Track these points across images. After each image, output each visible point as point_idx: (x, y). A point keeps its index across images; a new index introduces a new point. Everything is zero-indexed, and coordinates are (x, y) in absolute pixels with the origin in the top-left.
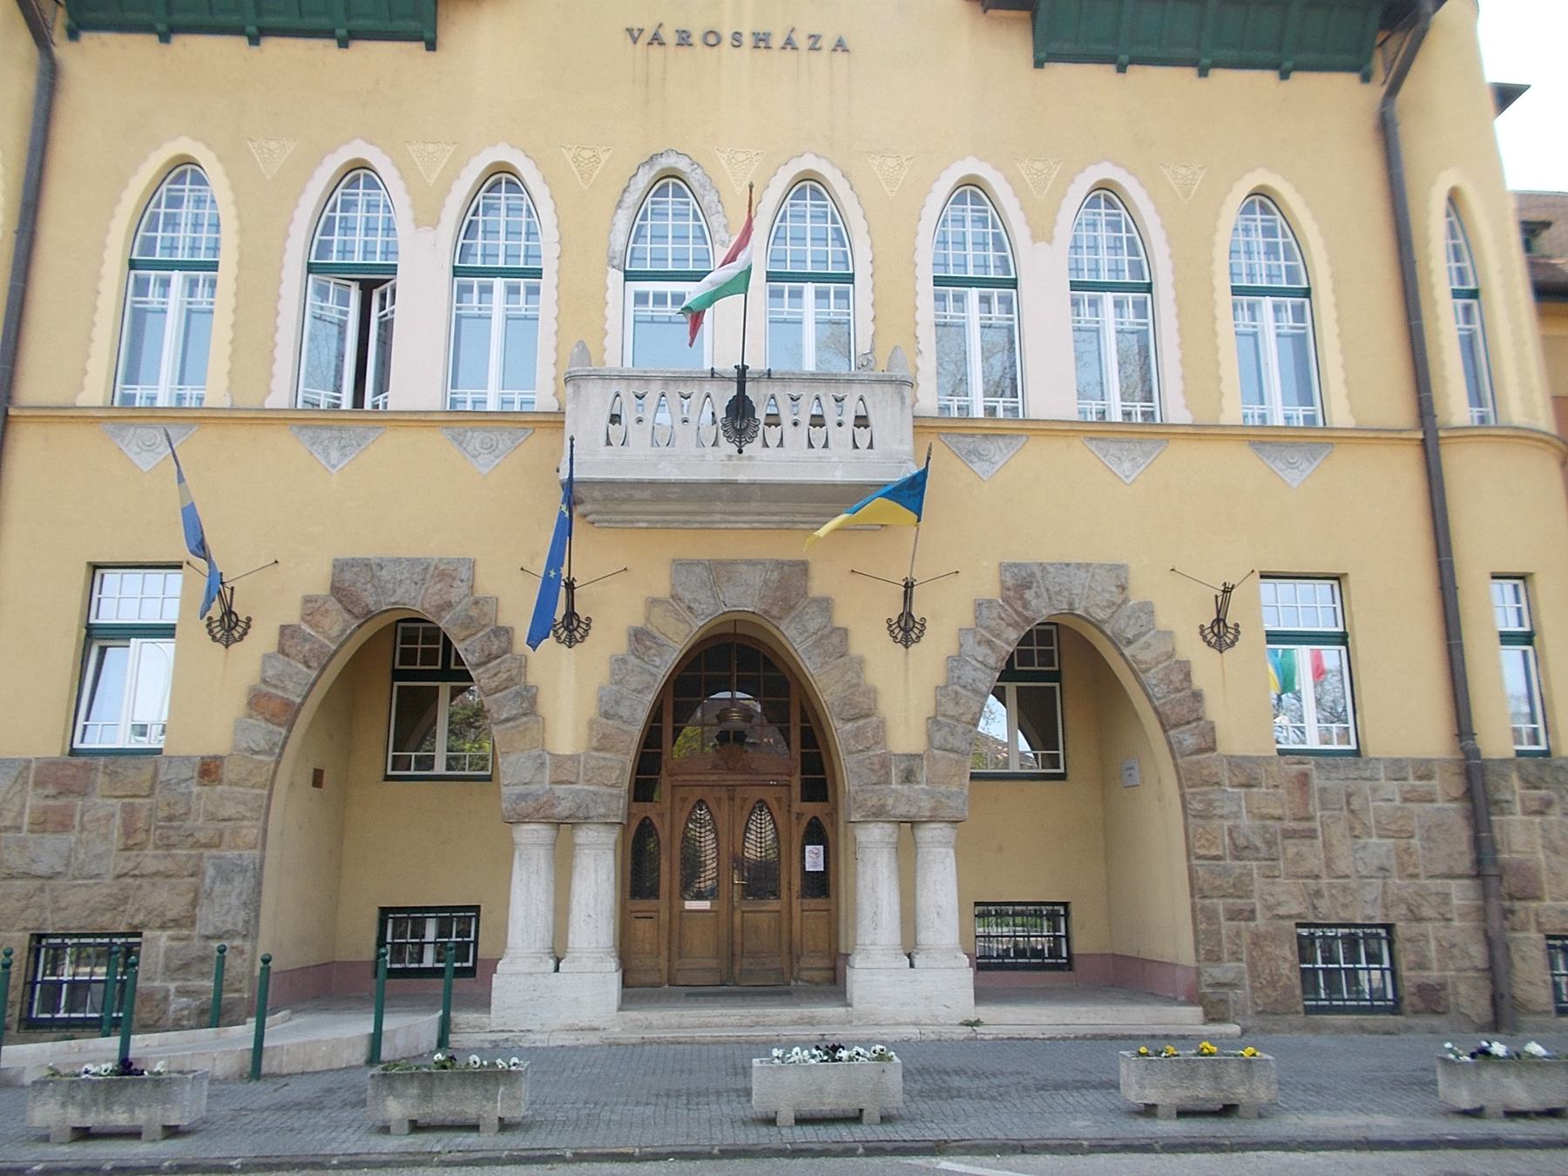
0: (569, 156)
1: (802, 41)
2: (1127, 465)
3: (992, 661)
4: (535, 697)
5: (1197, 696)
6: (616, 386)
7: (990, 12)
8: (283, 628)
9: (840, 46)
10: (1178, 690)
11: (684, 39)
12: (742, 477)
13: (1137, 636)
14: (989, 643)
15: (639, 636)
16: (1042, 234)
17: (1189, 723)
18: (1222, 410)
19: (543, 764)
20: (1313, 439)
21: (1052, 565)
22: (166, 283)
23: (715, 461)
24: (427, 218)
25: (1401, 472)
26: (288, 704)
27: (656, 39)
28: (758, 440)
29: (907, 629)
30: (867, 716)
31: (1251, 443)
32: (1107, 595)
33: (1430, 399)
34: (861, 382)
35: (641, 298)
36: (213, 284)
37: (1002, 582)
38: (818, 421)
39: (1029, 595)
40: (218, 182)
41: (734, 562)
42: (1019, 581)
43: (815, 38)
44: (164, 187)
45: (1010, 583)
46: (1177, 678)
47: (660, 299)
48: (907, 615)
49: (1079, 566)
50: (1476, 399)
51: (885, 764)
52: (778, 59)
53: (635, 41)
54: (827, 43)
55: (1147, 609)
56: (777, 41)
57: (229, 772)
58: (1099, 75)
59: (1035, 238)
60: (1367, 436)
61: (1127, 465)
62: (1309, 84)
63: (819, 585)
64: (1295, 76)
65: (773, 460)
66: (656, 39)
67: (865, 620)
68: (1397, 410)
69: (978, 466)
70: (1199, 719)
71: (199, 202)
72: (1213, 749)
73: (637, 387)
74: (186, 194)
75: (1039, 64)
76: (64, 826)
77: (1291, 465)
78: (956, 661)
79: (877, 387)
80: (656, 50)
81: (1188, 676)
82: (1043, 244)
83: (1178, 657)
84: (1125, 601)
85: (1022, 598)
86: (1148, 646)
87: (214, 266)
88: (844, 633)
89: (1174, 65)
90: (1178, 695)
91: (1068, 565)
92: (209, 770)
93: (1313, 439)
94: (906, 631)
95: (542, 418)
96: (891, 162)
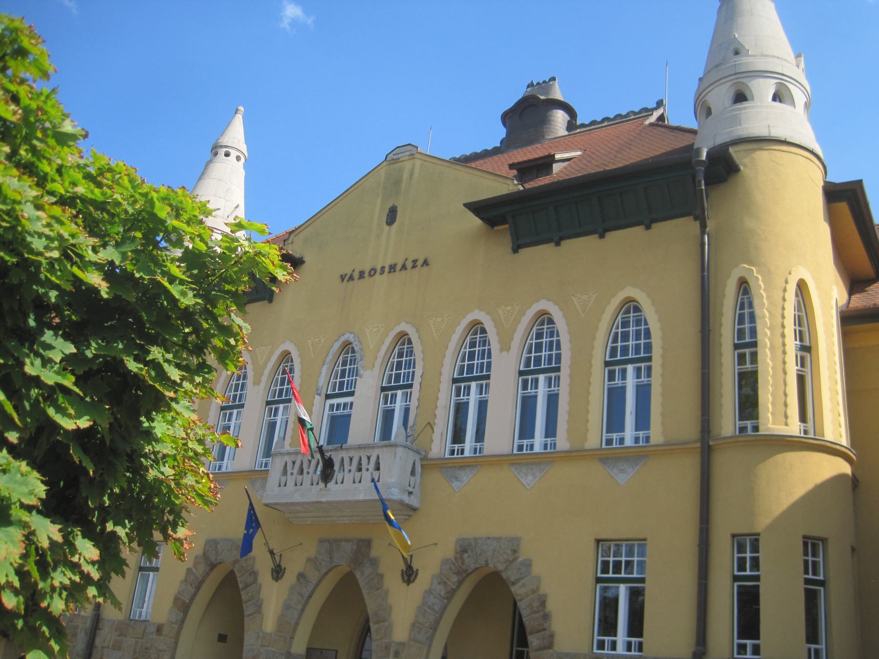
0: (310, 342)
1: (409, 264)
2: (530, 478)
3: (443, 594)
4: (261, 604)
5: (546, 617)
6: (286, 458)
7: (496, 228)
8: (188, 569)
9: (426, 263)
10: (535, 612)
11: (362, 275)
12: (323, 500)
13: (518, 580)
14: (445, 583)
15: (301, 576)
16: (505, 348)
17: (538, 632)
18: (586, 440)
19: (258, 637)
20: (641, 454)
21: (480, 538)
22: (624, 371)
23: (310, 491)
24: (505, 348)
25: (687, 469)
26: (184, 603)
27: (351, 278)
28: (333, 481)
29: (409, 575)
30: (383, 621)
31: (600, 459)
32: (505, 556)
33: (708, 421)
34: (379, 447)
35: (332, 407)
36: (649, 369)
37: (456, 549)
38: (301, 472)
39: (466, 555)
40: (561, 324)
41: (341, 540)
42: (464, 548)
43: (415, 261)
44: (620, 317)
45: (459, 550)
46: (536, 604)
47: (338, 406)
48: (409, 567)
49: (495, 538)
50: (803, 418)
51: (387, 647)
52: (399, 275)
53: (343, 280)
54: (419, 263)
55: (528, 564)
56: (399, 267)
57: (165, 631)
58: (545, 251)
59: (501, 350)
60: (670, 448)
61: (530, 478)
62: (661, 228)
63: (374, 553)
64: (654, 225)
65: (349, 488)
66: (351, 278)
67: (391, 570)
68: (690, 430)
69: (455, 484)
70: (544, 630)
71: (638, 322)
72: (550, 646)
73: (293, 458)
74: (631, 319)
75: (516, 249)
76: (119, 649)
77: (622, 471)
78: (429, 592)
79: (385, 449)
80: (351, 283)
81: (543, 603)
82: (505, 353)
83: (541, 592)
84: (515, 559)
85: (462, 558)
86: (524, 585)
87: (649, 359)
88: (381, 576)
89: (587, 235)
90: (536, 615)
91: (489, 538)
92: (159, 629)
93: (641, 454)
94: (409, 576)
95: (563, 455)
96: (439, 319)
